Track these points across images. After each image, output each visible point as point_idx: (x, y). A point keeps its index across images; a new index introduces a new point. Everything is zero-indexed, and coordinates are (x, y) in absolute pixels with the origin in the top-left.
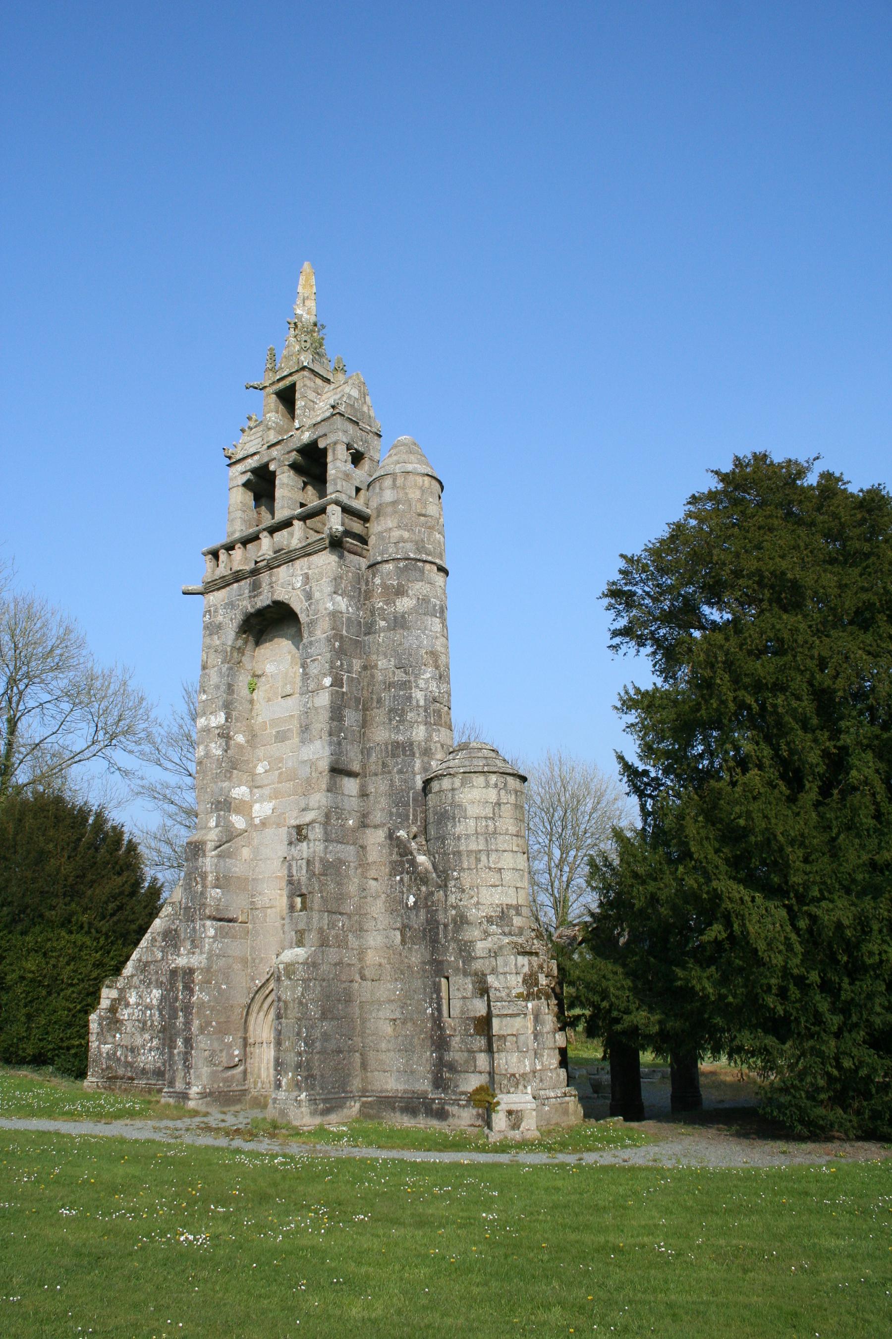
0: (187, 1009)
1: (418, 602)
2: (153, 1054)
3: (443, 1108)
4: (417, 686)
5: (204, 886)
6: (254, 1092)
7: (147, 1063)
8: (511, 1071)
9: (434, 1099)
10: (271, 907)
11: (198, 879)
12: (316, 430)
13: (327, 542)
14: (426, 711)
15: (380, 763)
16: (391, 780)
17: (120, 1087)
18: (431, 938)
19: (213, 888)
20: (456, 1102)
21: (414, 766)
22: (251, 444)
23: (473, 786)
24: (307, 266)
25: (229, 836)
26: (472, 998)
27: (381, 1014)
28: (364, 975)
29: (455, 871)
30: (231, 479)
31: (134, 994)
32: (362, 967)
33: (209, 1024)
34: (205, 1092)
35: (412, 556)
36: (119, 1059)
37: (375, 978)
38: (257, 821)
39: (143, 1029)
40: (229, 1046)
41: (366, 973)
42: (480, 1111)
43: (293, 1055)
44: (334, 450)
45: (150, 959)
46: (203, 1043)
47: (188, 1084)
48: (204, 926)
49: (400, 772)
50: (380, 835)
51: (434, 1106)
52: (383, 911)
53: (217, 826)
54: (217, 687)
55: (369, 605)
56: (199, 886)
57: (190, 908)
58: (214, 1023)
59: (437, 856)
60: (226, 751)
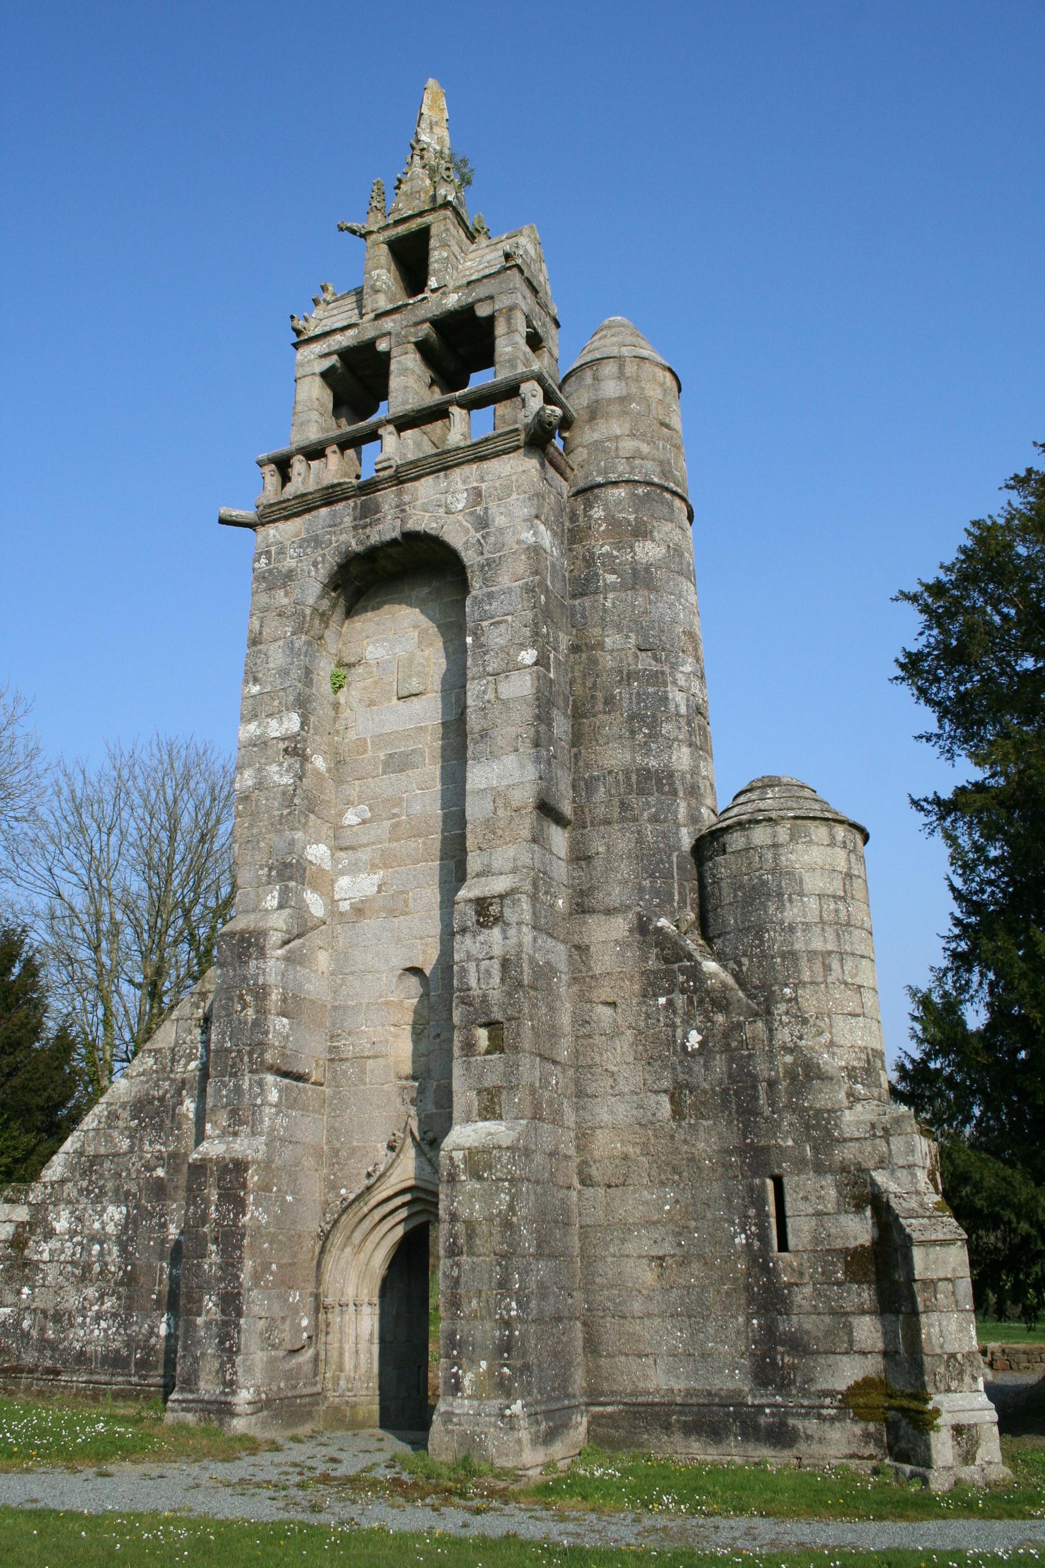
0: (231, 1239)
1: (668, 552)
2: (103, 1324)
3: (783, 1424)
4: (674, 683)
5: (262, 1011)
6: (333, 1398)
7: (89, 1342)
8: (949, 1348)
9: (761, 1407)
10: (376, 1057)
11: (248, 998)
12: (472, 290)
13: (522, 437)
14: (689, 724)
15: (616, 802)
16: (639, 832)
17: (28, 1388)
18: (739, 1105)
19: (278, 1015)
20: (813, 1411)
21: (676, 812)
22: (337, 322)
23: (811, 841)
24: (431, 82)
25: (302, 928)
26: (838, 1213)
27: (630, 1248)
28: (590, 1177)
29: (786, 985)
30: (302, 365)
31: (65, 1214)
32: (584, 1162)
33: (266, 1267)
34: (260, 1400)
35: (656, 480)
36: (26, 1335)
37: (614, 1181)
38: (344, 906)
39: (83, 1279)
40: (295, 1310)
41: (594, 1171)
42: (872, 1427)
43: (488, 1325)
44: (509, 320)
45: (102, 1151)
46: (257, 1304)
47: (232, 1383)
48: (261, 1084)
49: (654, 819)
50: (620, 927)
51: (762, 1420)
52: (631, 1059)
53: (281, 907)
54: (284, 672)
55: (581, 550)
56: (250, 1012)
57: (228, 1051)
58: (274, 1266)
59: (745, 961)
60: (301, 779)
